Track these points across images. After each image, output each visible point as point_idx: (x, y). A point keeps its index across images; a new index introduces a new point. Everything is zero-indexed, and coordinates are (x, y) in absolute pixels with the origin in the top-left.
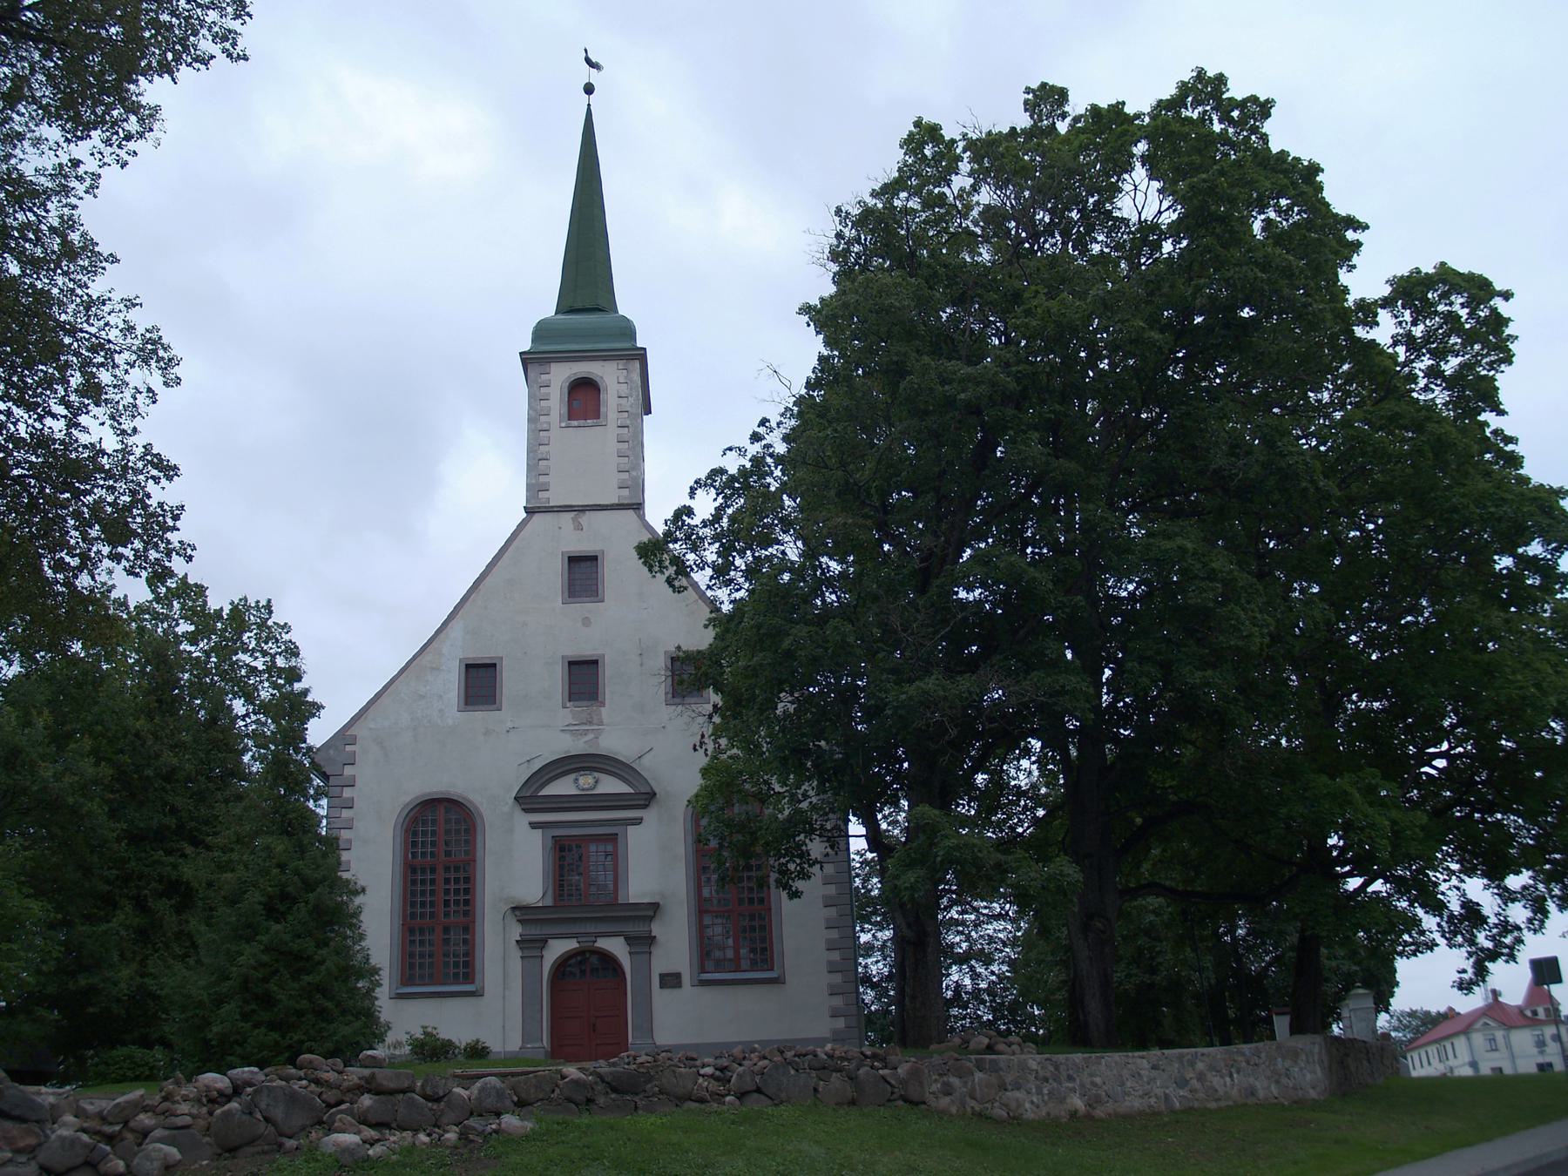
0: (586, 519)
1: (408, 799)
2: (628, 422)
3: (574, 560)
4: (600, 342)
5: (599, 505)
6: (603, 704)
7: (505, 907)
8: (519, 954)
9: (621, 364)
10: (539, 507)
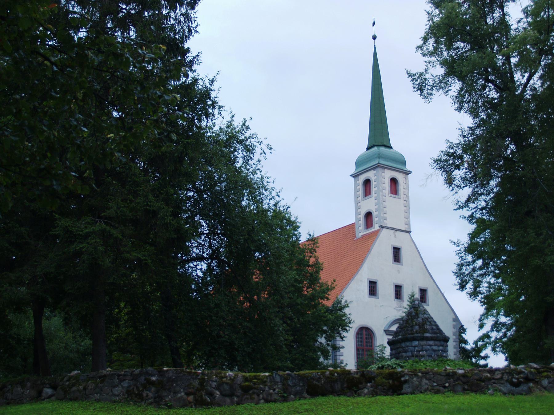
0: (398, 233)
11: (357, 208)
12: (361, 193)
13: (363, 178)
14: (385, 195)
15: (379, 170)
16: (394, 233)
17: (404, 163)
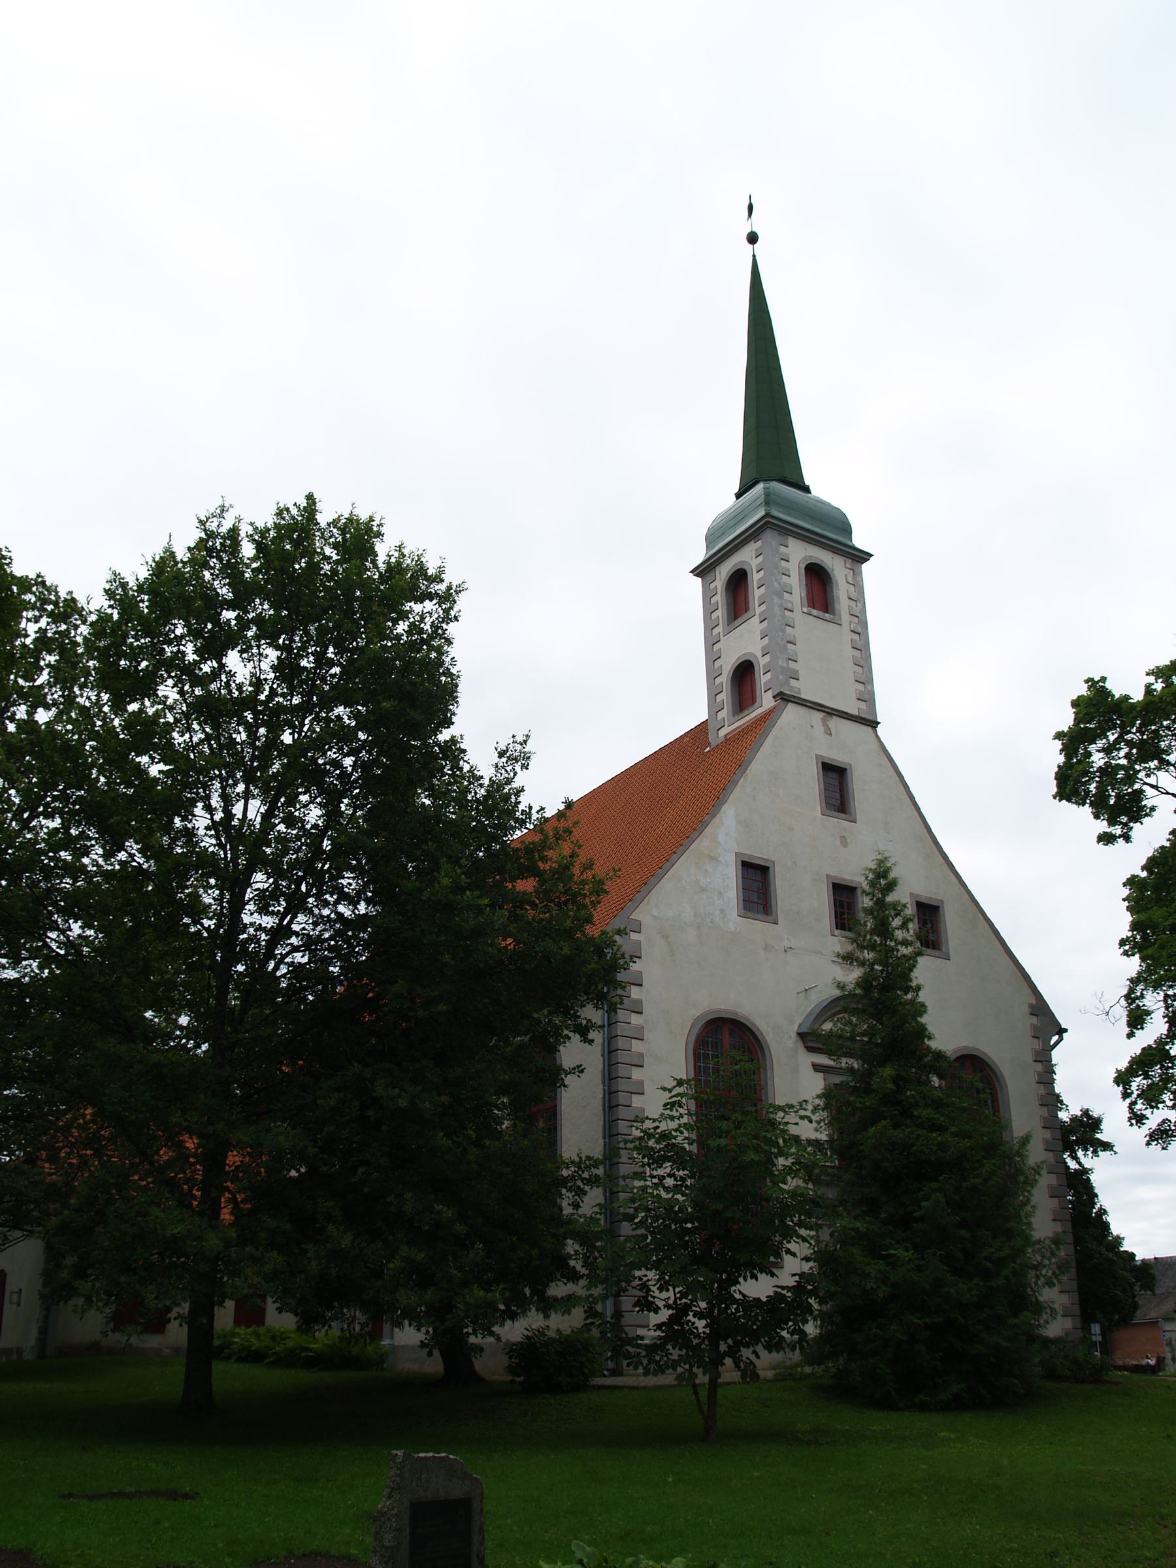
0: (835, 723)
4: (829, 531)
5: (846, 713)
10: (795, 697)
11: (712, 657)
12: (720, 614)
13: (724, 571)
14: (789, 606)
15: (770, 537)
16: (824, 721)
17: (846, 529)
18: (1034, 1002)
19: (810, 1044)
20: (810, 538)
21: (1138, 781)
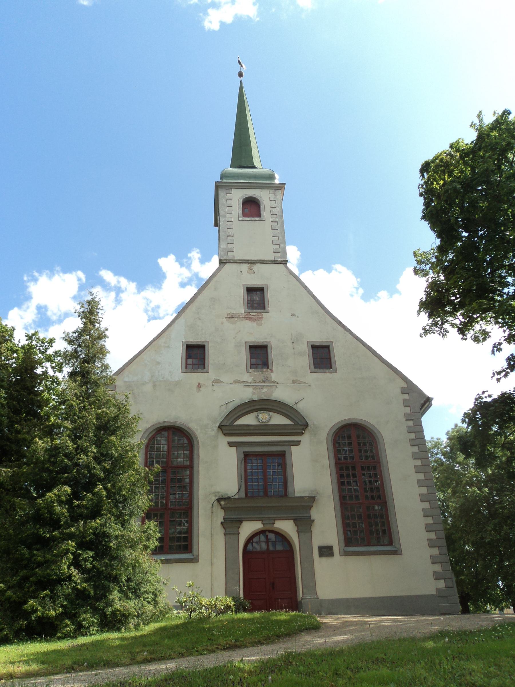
0: (257, 267)
1: (149, 426)
2: (277, 220)
3: (250, 290)
6: (272, 371)
7: (214, 498)
8: (223, 531)
9: (272, 191)
18: (405, 386)
19: (225, 432)
20: (237, 186)
21: (186, 477)
